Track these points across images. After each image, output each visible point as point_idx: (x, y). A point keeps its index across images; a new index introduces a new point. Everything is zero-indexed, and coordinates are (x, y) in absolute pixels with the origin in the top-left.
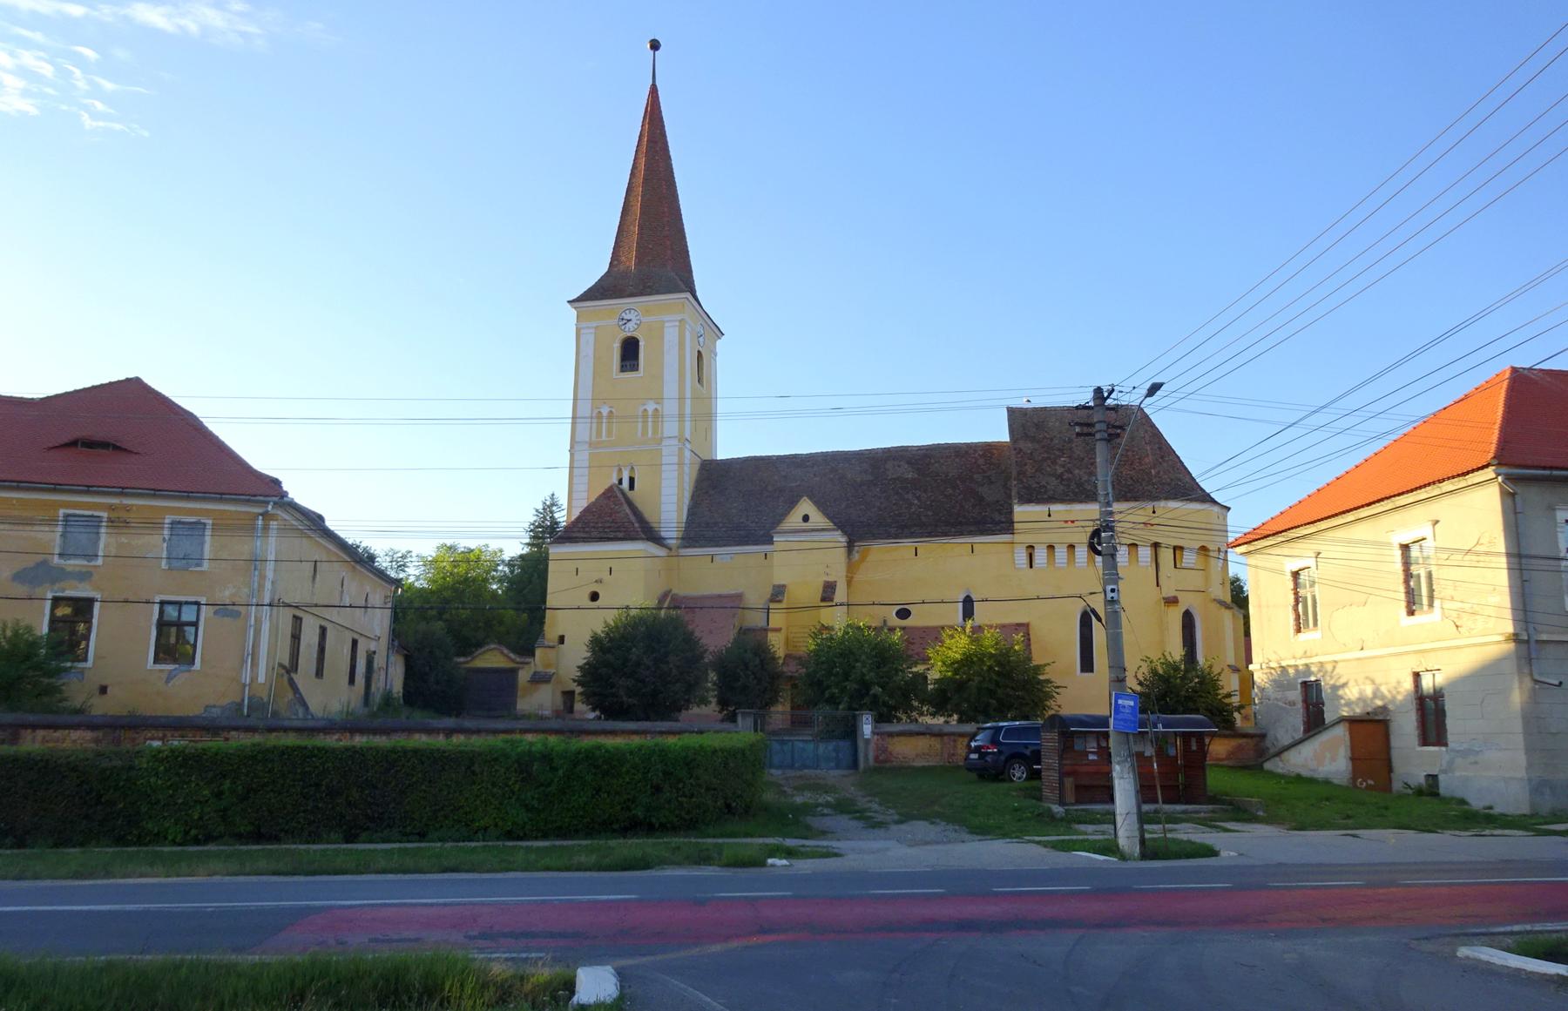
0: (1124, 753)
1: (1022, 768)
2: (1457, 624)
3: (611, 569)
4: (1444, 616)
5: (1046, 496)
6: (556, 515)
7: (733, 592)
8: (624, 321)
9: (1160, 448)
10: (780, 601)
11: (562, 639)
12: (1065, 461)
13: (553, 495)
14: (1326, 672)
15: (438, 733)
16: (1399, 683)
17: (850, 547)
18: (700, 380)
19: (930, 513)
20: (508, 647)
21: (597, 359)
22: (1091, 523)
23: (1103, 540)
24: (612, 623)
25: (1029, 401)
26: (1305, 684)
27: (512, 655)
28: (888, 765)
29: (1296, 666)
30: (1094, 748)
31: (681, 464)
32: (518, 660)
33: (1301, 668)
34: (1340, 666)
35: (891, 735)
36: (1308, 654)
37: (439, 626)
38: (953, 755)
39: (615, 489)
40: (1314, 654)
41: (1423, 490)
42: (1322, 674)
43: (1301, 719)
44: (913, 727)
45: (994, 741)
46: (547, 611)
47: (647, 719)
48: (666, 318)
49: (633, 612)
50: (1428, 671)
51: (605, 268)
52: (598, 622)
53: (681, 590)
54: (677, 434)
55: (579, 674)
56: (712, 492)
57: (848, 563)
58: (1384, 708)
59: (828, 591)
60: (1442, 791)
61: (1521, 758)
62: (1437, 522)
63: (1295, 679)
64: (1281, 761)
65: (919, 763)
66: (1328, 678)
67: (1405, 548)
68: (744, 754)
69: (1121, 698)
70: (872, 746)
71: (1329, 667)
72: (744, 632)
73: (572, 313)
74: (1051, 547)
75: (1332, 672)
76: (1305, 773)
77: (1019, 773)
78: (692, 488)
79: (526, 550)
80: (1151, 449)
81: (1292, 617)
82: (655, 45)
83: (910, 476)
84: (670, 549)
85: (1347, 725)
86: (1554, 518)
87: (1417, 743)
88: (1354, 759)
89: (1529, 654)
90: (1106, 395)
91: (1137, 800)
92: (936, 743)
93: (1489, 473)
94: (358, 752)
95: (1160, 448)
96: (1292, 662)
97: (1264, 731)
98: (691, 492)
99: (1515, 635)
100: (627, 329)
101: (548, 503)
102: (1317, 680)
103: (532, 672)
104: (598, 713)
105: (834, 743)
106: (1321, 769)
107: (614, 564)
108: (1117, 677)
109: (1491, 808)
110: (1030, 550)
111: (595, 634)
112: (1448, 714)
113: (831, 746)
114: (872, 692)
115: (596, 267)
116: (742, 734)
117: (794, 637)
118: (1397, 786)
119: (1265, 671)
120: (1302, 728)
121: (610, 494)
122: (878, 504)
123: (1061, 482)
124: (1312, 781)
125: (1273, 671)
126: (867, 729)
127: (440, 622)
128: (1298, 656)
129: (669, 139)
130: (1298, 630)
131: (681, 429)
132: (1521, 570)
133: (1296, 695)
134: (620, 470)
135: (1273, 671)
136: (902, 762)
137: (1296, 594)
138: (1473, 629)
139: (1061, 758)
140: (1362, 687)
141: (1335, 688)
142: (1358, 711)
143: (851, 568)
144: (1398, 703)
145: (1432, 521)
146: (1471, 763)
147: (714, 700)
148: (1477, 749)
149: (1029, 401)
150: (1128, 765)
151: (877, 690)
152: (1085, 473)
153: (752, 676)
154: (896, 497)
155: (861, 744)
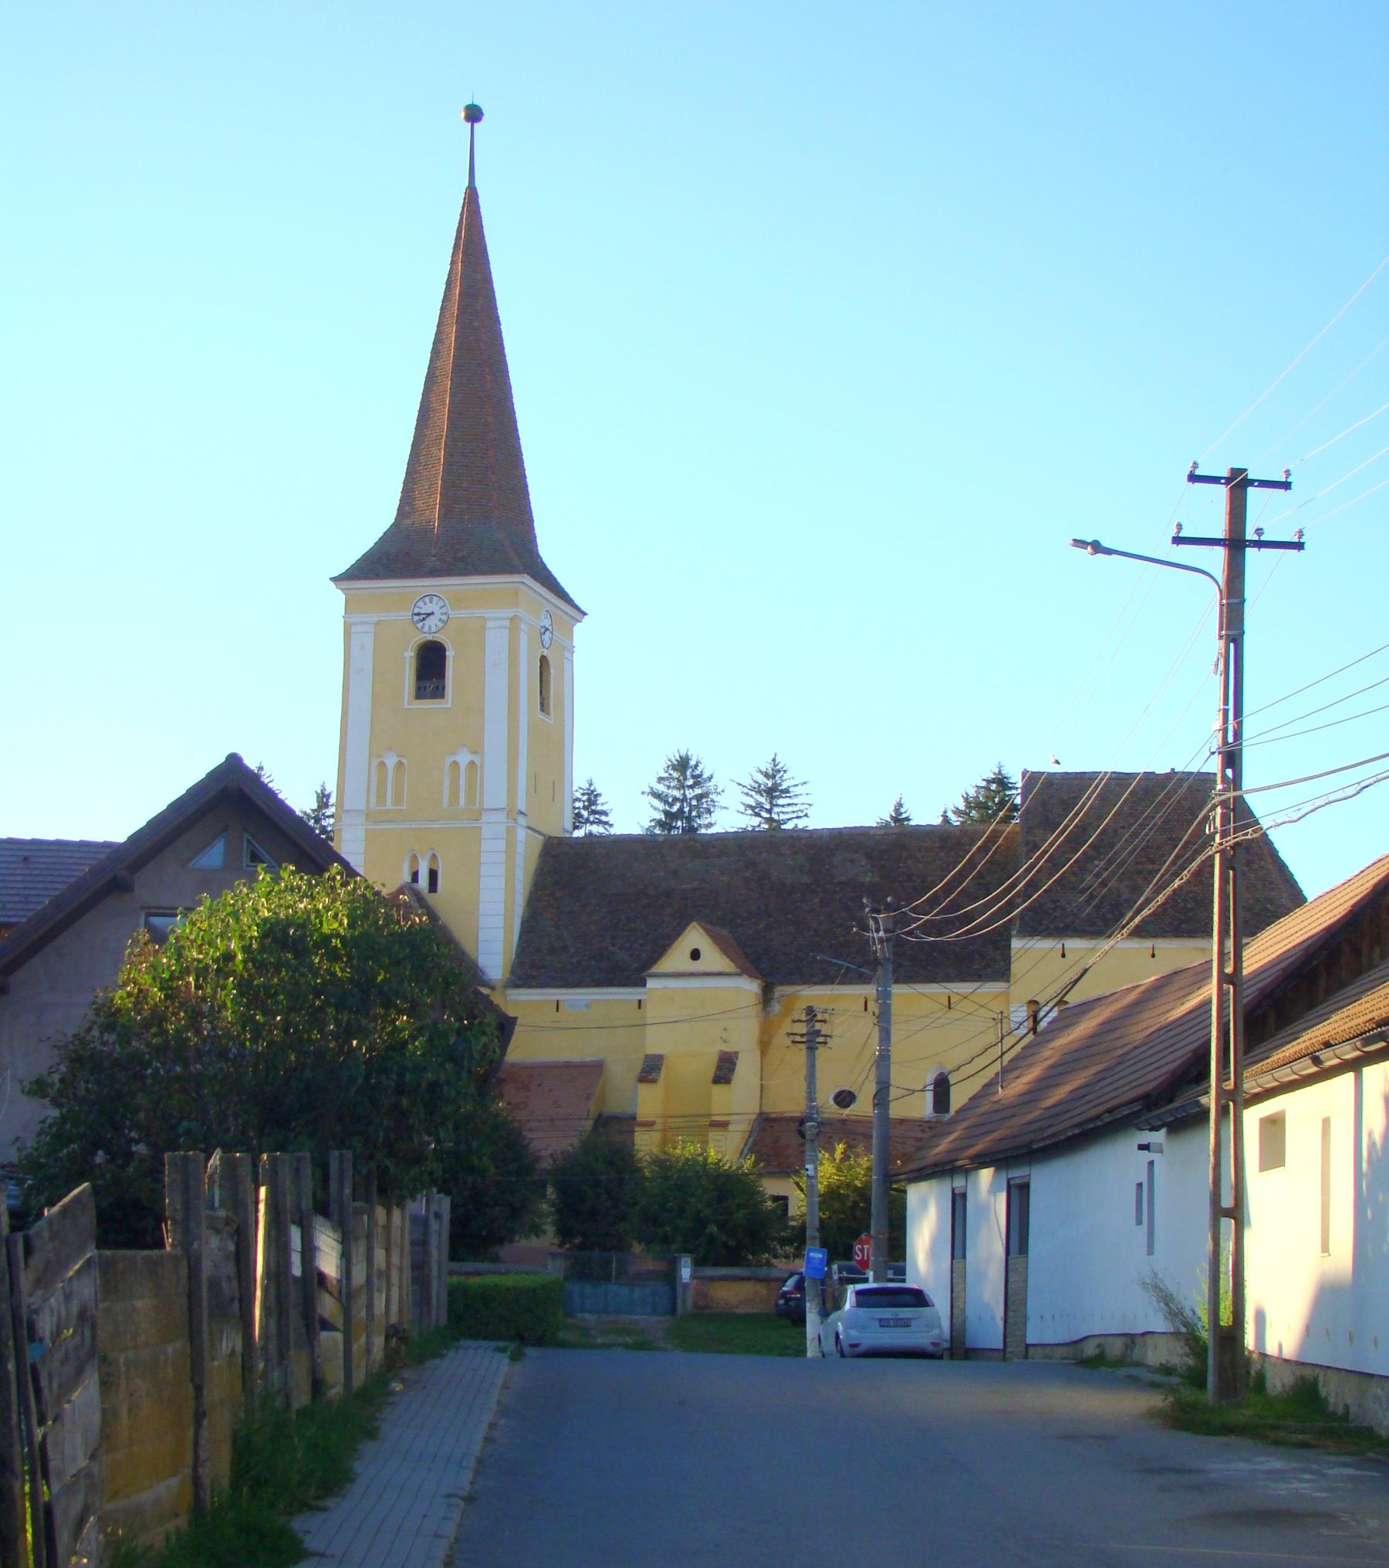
7: (588, 1059)
8: (421, 617)
17: (766, 997)
18: (544, 706)
25: (1057, 762)
31: (510, 852)
35: (712, 1279)
54: (504, 805)
59: (725, 1069)
65: (740, 1310)
72: (604, 1121)
73: (337, 598)
82: (473, 114)
100: (426, 629)
110: (1034, 1008)
126: (686, 1273)
134: (414, 859)
147: (550, 1229)
149: (1057, 762)
150: (815, 1302)
151: (713, 1229)
152: (1127, 886)
155: (679, 1289)
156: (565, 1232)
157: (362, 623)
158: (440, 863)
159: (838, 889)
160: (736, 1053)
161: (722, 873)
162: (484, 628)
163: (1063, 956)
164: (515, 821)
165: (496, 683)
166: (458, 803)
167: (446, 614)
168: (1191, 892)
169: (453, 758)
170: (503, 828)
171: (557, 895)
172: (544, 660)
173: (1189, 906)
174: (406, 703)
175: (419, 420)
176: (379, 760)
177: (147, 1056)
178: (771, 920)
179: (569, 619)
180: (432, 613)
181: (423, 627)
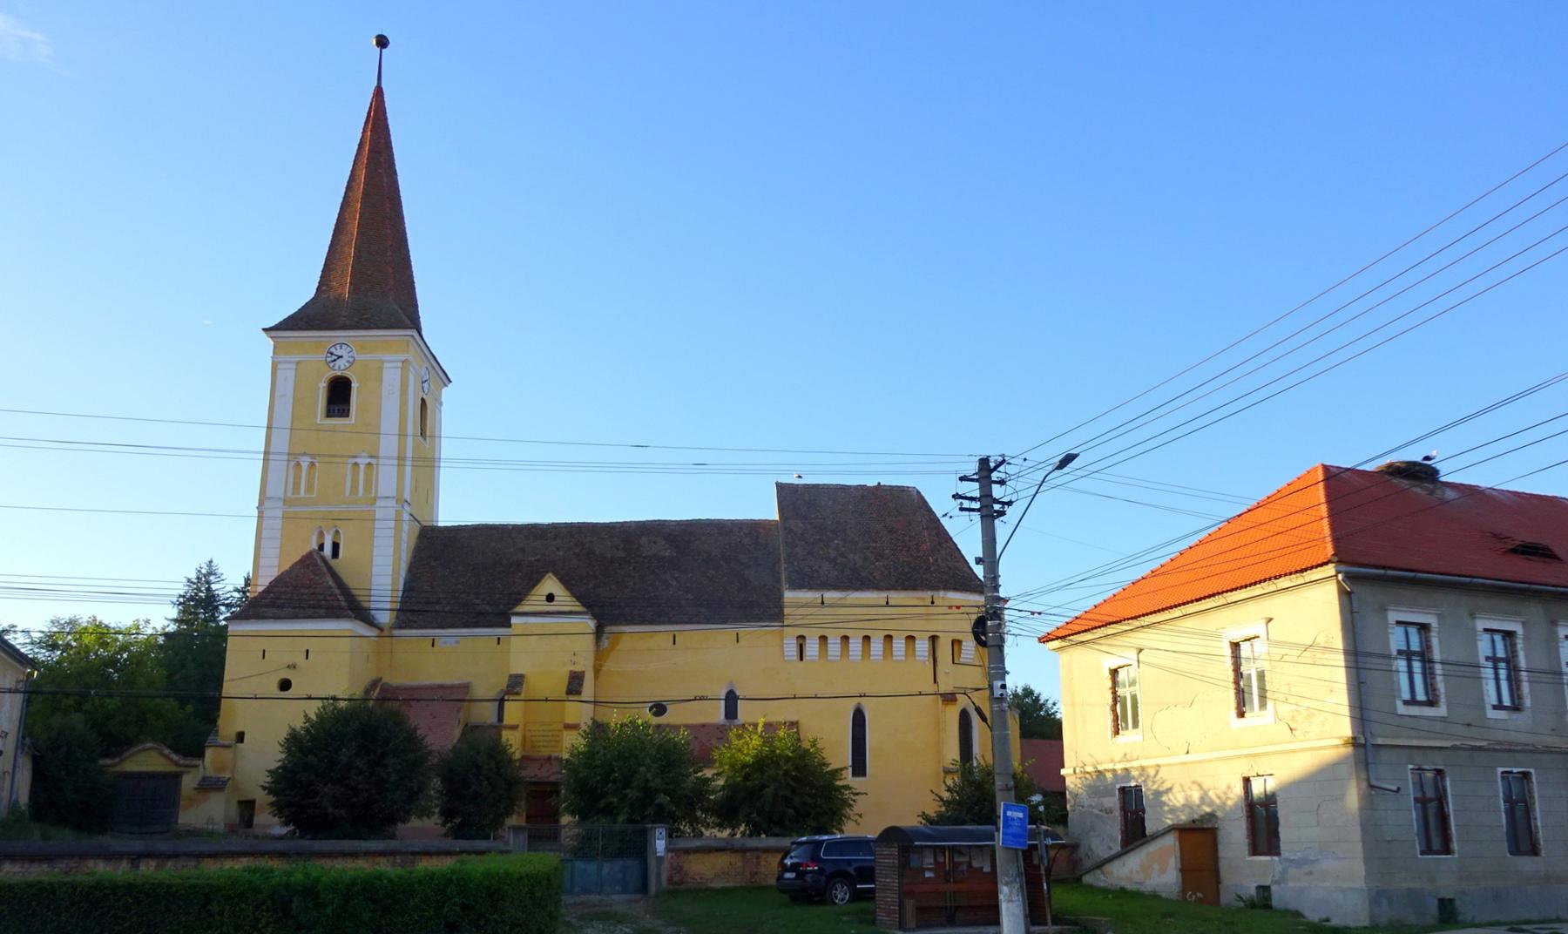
0: (1013, 872)
1: (845, 887)
2: (1292, 727)
3: (433, 646)
4: (1278, 718)
5: (819, 582)
6: (214, 587)
7: (456, 682)
8: (335, 357)
9: (937, 534)
10: (518, 694)
11: (240, 737)
12: (838, 544)
13: (211, 562)
14: (1148, 776)
15: (121, 859)
16: (1229, 787)
17: (599, 633)
18: (423, 433)
19: (690, 596)
20: (170, 747)
21: (297, 401)
22: (976, 610)
23: (988, 630)
24: (314, 717)
25: (800, 477)
26: (1123, 790)
27: (175, 757)
28: (683, 887)
29: (1114, 770)
30: (931, 864)
31: (397, 541)
32: (182, 762)
33: (1119, 772)
34: (1162, 769)
35: (687, 851)
36: (1128, 757)
37: (77, 718)
38: (756, 873)
39: (316, 556)
40: (1135, 758)
41: (1258, 586)
42: (1143, 778)
43: (1119, 827)
44: (697, 843)
45: (815, 859)
46: (223, 700)
47: (358, 837)
48: (386, 357)
49: (342, 704)
50: (1259, 776)
51: (310, 293)
52: (295, 715)
53: (395, 679)
54: (395, 495)
55: (269, 779)
56: (433, 564)
57: (597, 651)
58: (1212, 815)
59: (575, 683)
60: (1275, 903)
61: (1359, 867)
62: (1271, 620)
63: (1113, 784)
64: (1103, 873)
65: (718, 885)
66: (1150, 783)
67: (1235, 646)
68: (549, 880)
69: (1011, 810)
70: (666, 866)
71: (1152, 772)
72: (470, 729)
74: (911, 638)
75: (1155, 776)
76: (1129, 886)
77: (841, 893)
78: (409, 558)
79: (172, 628)
80: (930, 535)
81: (1109, 717)
83: (667, 554)
84: (381, 630)
85: (1177, 834)
86: (1386, 619)
87: (1247, 852)
88: (1184, 871)
89: (1366, 759)
90: (992, 465)
91: (1026, 924)
92: (737, 860)
93: (1330, 570)
94: (45, 888)
95: (937, 534)
96: (1111, 766)
97: (1077, 841)
98: (409, 562)
99: (1354, 738)
100: (336, 367)
101: (204, 571)
102: (1136, 786)
103: (200, 777)
104: (291, 827)
105: (621, 862)
106: (1148, 882)
107: (310, 644)
108: (1007, 785)
109: (1328, 920)
110: (800, 641)
111: (293, 730)
112: (1282, 821)
113: (618, 865)
114: (657, 801)
115: (301, 290)
116: (543, 860)
117: (532, 736)
118: (1226, 897)
119: (1078, 776)
120: (1120, 837)
121: (310, 562)
122: (631, 584)
123: (834, 567)
124: (1138, 895)
125: (1087, 776)
127: (78, 714)
128: (1117, 759)
129: (395, 151)
130: (1117, 732)
131: (400, 489)
132: (1357, 668)
133: (1113, 802)
134: (321, 534)
135: (1087, 776)
136: (699, 883)
137: (1114, 692)
138: (1308, 733)
139: (901, 876)
140: (1189, 792)
141: (1158, 794)
142: (1183, 818)
143: (600, 656)
144: (1228, 809)
145: (1266, 618)
146: (1307, 874)
148: (1312, 858)
150: (1017, 886)
153: (486, 782)
154: (652, 577)
155: (652, 864)
156: (447, 814)
157: (286, 362)
160: (584, 672)
161: (558, 549)
162: (381, 368)
164: (403, 507)
167: (352, 357)
172: (423, 400)
175: (335, 231)
177: (64, 654)
179: (440, 382)
180: (341, 357)
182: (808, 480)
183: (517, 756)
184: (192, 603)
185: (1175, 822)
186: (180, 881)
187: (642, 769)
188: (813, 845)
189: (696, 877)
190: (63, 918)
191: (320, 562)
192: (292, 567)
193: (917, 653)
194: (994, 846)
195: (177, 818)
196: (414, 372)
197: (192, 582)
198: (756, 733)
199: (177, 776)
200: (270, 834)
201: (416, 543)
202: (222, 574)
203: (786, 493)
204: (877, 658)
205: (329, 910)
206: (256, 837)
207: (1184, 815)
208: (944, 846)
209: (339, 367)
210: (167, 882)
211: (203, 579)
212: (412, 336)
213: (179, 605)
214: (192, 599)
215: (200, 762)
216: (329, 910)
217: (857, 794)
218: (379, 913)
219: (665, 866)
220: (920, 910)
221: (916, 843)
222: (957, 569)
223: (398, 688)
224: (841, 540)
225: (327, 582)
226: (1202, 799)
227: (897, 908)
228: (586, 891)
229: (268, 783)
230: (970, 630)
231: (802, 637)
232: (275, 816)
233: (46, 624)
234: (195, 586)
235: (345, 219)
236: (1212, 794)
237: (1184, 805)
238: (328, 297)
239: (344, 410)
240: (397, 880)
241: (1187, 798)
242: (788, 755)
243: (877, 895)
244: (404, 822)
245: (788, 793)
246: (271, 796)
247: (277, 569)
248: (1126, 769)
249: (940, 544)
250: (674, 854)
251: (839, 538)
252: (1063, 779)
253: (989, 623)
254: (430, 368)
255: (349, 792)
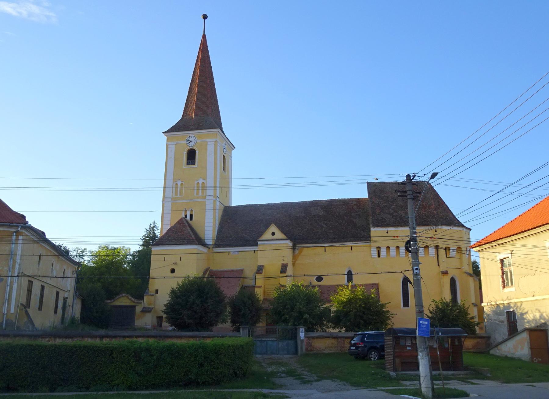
5: (386, 224)
6: (156, 232)
8: (190, 142)
11: (157, 291)
13: (154, 222)
14: (518, 307)
17: (294, 248)
18: (224, 169)
19: (331, 231)
23: (411, 246)
24: (181, 284)
25: (377, 179)
26: (508, 312)
27: (133, 299)
28: (312, 352)
30: (409, 344)
31: (215, 209)
33: (506, 305)
34: (524, 304)
35: (313, 338)
36: (509, 298)
38: (343, 347)
39: (183, 220)
45: (362, 341)
51: (180, 117)
52: (174, 284)
54: (213, 194)
55: (165, 308)
58: (545, 324)
59: (284, 268)
63: (503, 310)
64: (498, 349)
66: (518, 310)
68: (243, 348)
69: (422, 321)
71: (519, 305)
72: (244, 288)
74: (388, 248)
75: (521, 306)
82: (205, 17)
85: (528, 332)
88: (532, 348)
92: (334, 342)
94: (57, 347)
96: (502, 302)
100: (190, 145)
102: (513, 311)
103: (142, 307)
106: (516, 353)
110: (378, 249)
111: (173, 289)
113: (285, 343)
114: (304, 317)
115: (177, 116)
117: (267, 290)
120: (507, 334)
121: (181, 222)
123: (392, 217)
124: (512, 359)
125: (493, 306)
127: (99, 283)
128: (505, 299)
133: (504, 318)
134: (186, 211)
135: (493, 306)
137: (502, 270)
139: (394, 349)
140: (535, 314)
141: (522, 314)
143: (295, 257)
150: (425, 353)
152: (403, 212)
155: (299, 342)
156: (234, 322)
158: (194, 212)
159: (313, 217)
160: (287, 264)
162: (207, 144)
163: (387, 233)
165: (210, 160)
166: (199, 194)
168: (424, 213)
169: (197, 182)
170: (213, 201)
171: (228, 222)
173: (424, 217)
174: (184, 166)
176: (176, 183)
178: (294, 226)
180: (192, 141)
181: (189, 145)
182: (380, 181)
183: (261, 298)
184: (148, 239)
185: (530, 327)
186: (103, 345)
187: (298, 304)
188: (362, 336)
189: (318, 348)
190: (63, 358)
191: (185, 222)
192: (175, 225)
193: (430, 253)
194: (416, 336)
195: (134, 323)
196: (219, 145)
197: (147, 230)
198: (348, 289)
199: (134, 307)
200: (168, 330)
201: (223, 213)
202: (159, 227)
203: (370, 186)
204: (402, 256)
205: (155, 357)
206: (164, 331)
207: (533, 323)
208: (448, 336)
209: (191, 145)
210: (98, 345)
211: (152, 229)
212: (218, 131)
213: (143, 239)
214: (147, 237)
215: (142, 301)
216: (155, 357)
217: (392, 314)
218: (174, 359)
219: (304, 343)
220: (402, 363)
221: (399, 335)
222: (447, 216)
223: (216, 271)
224: (395, 205)
225: (188, 230)
226: (540, 317)
227: (393, 362)
228: (272, 353)
229: (164, 309)
230: (404, 246)
231: (379, 248)
232: (167, 322)
233: (97, 248)
234: (149, 232)
235: (192, 87)
236: (544, 315)
237: (533, 320)
238: (187, 118)
239: (193, 162)
240: (180, 346)
241: (534, 316)
242: (361, 298)
243: (385, 356)
244: (216, 325)
245: (361, 314)
246: (165, 315)
247: (170, 225)
248: (508, 303)
249: (439, 205)
250: (308, 339)
251: (394, 205)
252: (483, 308)
253: (412, 243)
254: (226, 143)
255: (194, 313)
